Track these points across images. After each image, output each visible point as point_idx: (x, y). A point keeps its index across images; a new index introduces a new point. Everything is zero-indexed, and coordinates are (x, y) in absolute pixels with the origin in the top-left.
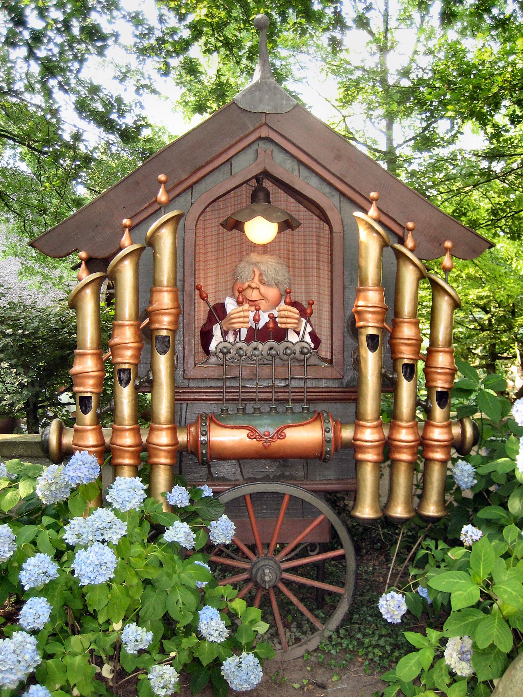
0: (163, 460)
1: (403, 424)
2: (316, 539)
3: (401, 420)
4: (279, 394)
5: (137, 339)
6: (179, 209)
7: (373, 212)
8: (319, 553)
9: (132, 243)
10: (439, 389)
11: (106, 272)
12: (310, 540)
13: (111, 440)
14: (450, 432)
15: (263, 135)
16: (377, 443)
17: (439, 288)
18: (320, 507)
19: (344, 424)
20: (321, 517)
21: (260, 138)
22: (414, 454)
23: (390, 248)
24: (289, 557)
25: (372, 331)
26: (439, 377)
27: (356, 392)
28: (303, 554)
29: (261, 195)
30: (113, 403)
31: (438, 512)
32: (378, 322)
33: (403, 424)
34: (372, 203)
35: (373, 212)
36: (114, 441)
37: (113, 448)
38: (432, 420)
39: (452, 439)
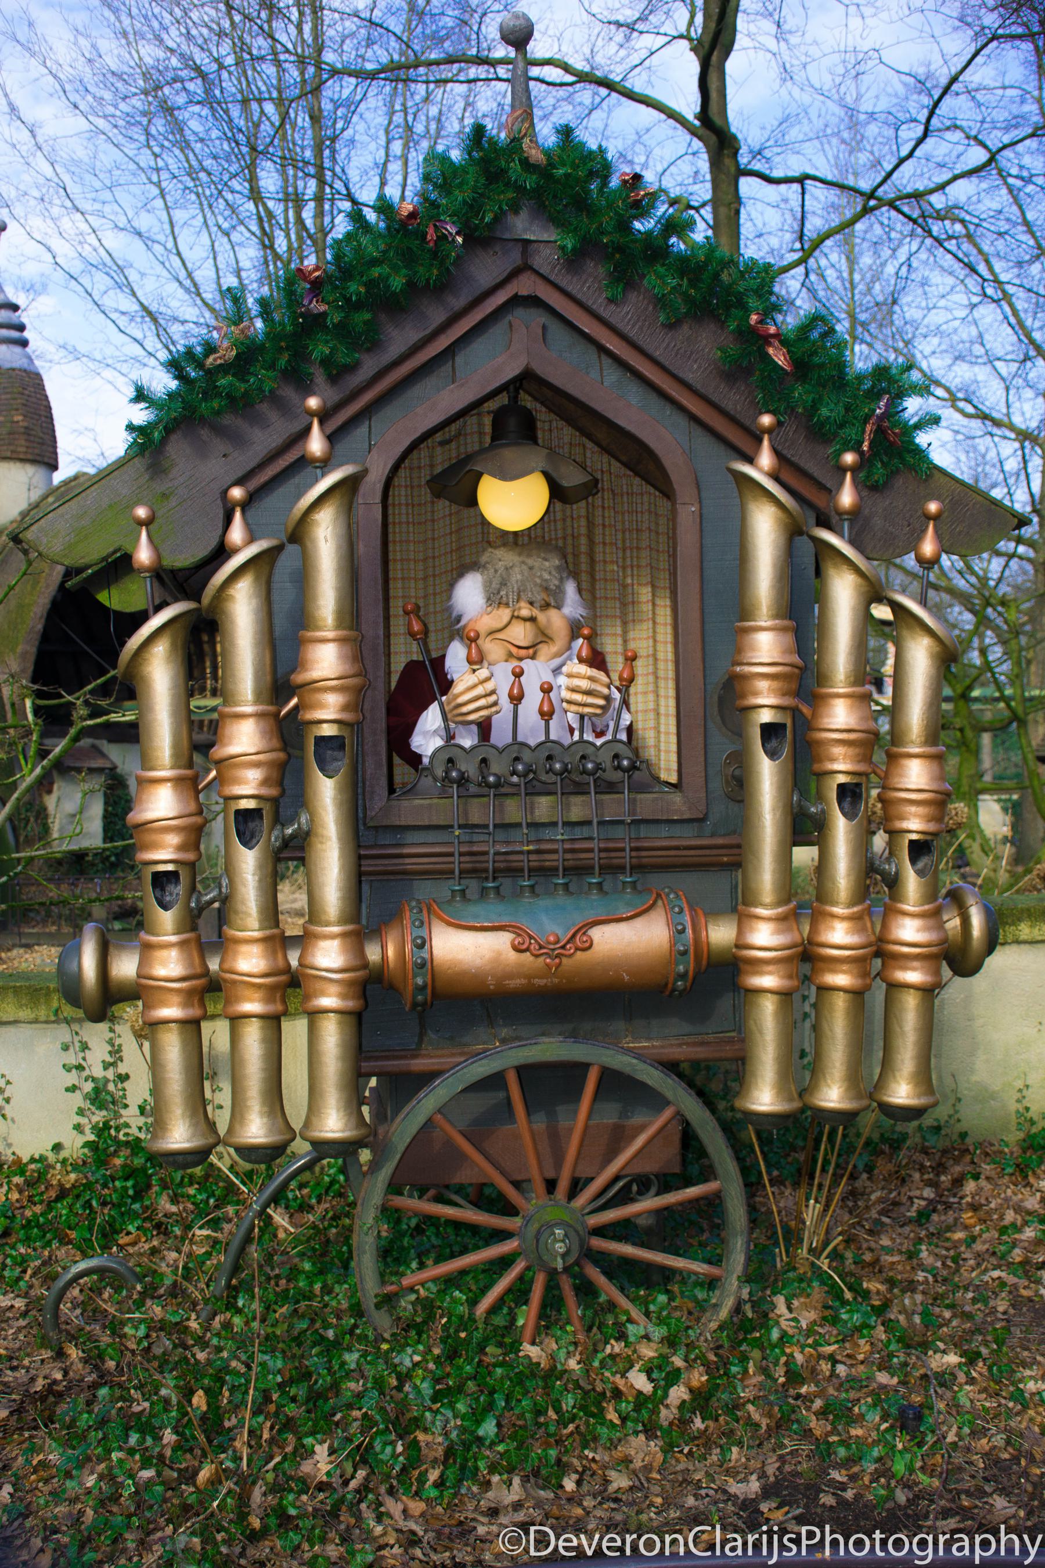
0: (328, 1001)
1: (837, 910)
2: (648, 1167)
3: (835, 903)
4: (613, 854)
5: (276, 743)
6: (355, 462)
7: (766, 459)
8: (657, 1194)
9: (251, 539)
10: (914, 837)
11: (199, 602)
12: (638, 1169)
13: (299, 960)
14: (940, 926)
15: (524, 292)
16: (194, 982)
17: (911, 621)
18: (669, 1094)
19: (715, 913)
20: (668, 1113)
21: (516, 301)
22: (864, 974)
23: (805, 537)
24: (601, 1201)
25: (766, 716)
26: (913, 809)
27: (739, 846)
28: (624, 1197)
29: (512, 423)
30: (225, 882)
31: (919, 1096)
32: (784, 694)
33: (837, 910)
34: (760, 441)
35: (766, 459)
36: (146, 971)
37: (225, 981)
38: (900, 901)
39: (944, 941)
